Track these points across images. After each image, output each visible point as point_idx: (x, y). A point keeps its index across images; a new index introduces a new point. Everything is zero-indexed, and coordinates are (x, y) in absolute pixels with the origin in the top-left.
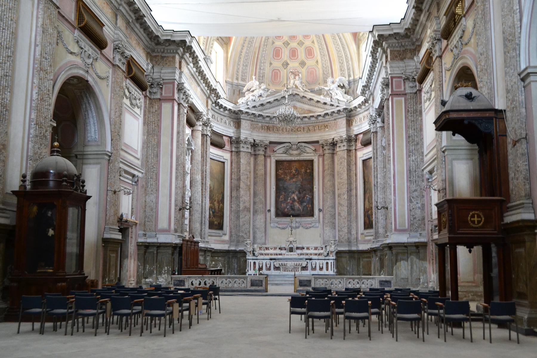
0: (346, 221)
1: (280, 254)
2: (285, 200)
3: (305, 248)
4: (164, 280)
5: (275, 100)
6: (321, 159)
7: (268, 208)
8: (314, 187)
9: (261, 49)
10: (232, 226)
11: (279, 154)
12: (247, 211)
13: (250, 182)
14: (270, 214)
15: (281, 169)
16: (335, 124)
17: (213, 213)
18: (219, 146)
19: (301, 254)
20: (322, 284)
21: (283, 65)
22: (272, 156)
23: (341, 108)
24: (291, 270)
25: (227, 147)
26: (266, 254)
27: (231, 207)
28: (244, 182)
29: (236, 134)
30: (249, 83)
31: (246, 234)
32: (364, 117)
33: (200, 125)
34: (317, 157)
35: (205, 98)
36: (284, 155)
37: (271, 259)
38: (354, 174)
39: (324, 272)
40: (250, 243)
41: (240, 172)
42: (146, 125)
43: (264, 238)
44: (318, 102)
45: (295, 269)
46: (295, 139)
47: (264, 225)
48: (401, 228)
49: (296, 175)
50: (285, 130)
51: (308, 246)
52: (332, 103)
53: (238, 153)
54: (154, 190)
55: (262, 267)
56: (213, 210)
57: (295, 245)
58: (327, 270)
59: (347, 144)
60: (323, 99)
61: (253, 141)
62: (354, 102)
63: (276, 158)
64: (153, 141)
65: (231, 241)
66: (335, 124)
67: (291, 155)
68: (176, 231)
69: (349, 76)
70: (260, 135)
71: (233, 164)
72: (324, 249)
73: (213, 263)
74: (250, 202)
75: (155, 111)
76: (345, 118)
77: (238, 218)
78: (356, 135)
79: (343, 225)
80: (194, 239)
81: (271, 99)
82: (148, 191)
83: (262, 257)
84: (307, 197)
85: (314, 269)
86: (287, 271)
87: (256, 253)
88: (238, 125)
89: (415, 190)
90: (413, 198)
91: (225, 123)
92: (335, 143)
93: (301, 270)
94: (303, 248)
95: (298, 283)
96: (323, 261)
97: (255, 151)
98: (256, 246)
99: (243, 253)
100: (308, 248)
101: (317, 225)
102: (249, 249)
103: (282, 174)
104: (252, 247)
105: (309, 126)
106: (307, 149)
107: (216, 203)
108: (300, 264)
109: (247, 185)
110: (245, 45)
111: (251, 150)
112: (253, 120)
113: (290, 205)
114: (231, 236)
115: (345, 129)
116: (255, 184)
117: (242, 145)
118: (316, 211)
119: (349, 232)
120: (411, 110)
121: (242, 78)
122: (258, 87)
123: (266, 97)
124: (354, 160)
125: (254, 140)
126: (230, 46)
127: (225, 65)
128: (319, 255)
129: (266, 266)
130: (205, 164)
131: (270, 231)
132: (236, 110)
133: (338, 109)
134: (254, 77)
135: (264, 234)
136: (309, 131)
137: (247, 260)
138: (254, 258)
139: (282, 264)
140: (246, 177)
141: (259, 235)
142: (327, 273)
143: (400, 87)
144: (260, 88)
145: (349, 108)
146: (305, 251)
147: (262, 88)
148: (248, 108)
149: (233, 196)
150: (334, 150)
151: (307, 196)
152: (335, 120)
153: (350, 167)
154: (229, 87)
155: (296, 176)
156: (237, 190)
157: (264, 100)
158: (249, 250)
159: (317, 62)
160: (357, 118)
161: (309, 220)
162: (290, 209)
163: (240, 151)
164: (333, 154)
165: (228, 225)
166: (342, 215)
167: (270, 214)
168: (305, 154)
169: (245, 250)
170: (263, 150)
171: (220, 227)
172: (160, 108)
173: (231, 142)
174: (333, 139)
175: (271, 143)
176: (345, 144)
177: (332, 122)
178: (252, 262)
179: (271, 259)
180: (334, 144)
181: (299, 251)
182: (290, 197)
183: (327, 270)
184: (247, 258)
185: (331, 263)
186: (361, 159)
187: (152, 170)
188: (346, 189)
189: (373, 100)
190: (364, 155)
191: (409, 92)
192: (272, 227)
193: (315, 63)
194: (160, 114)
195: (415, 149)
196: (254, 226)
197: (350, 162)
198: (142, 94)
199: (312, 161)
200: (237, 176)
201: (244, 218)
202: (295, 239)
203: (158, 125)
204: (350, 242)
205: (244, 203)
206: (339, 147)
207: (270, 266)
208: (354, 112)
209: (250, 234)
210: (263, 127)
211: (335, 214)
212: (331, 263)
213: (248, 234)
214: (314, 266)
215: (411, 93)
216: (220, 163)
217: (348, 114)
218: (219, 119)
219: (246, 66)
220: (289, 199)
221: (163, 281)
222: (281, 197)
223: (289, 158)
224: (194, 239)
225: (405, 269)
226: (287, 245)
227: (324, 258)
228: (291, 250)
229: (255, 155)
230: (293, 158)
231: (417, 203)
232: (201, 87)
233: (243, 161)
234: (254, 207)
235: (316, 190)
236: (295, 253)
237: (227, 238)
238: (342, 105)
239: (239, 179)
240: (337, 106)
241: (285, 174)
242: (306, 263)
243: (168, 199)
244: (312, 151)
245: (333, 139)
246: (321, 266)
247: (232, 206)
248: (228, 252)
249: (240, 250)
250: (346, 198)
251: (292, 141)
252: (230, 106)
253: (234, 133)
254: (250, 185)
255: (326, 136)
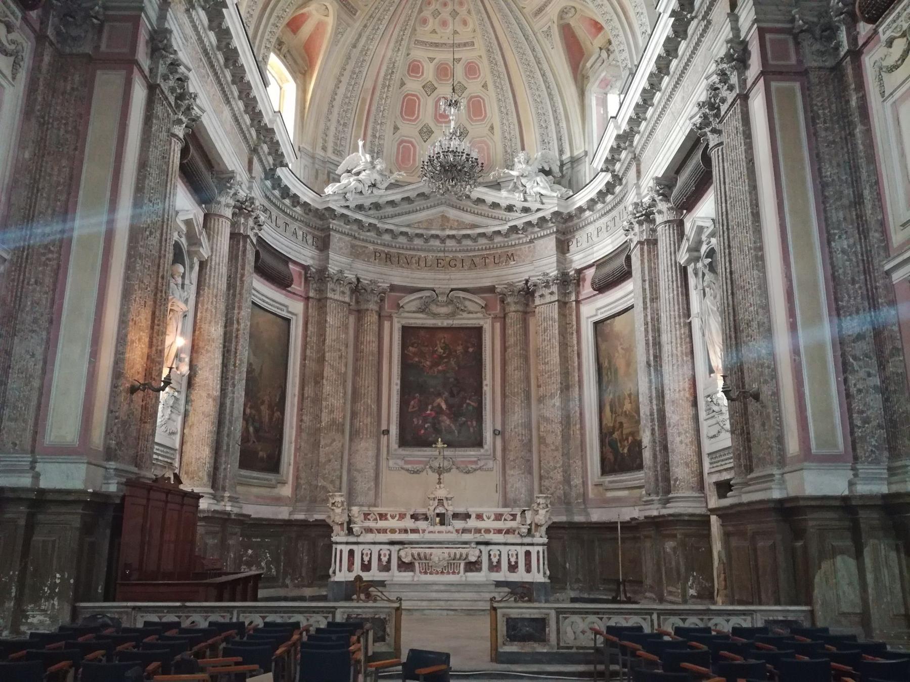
0: (558, 454)
1: (414, 531)
2: (422, 407)
3: (473, 516)
4: (47, 621)
5: (403, 199)
6: (498, 325)
7: (384, 427)
8: (484, 383)
9: (377, 93)
10: (301, 465)
11: (408, 312)
12: (337, 430)
13: (346, 366)
14: (388, 440)
15: (412, 346)
16: (530, 251)
17: (256, 431)
18: (281, 281)
19: (465, 531)
20: (583, 632)
21: (420, 132)
22: (394, 315)
23: (547, 214)
24: (439, 570)
25: (298, 287)
26: (379, 531)
27: (302, 420)
28: (332, 367)
29: (318, 262)
30: (351, 155)
31: (332, 482)
32: (599, 231)
33: (227, 205)
34: (489, 321)
35: (246, 150)
36: (421, 315)
37: (392, 543)
38: (576, 352)
39: (521, 576)
40: (342, 503)
41: (324, 344)
42: (33, 120)
43: (372, 493)
44: (495, 205)
45: (450, 566)
46: (445, 282)
47: (373, 463)
48: (825, 451)
49: (445, 357)
50: (422, 264)
51: (479, 510)
52: (526, 205)
53: (322, 302)
54: (43, 321)
55: (370, 561)
56: (257, 425)
57: (450, 508)
58: (528, 570)
59: (559, 290)
60: (506, 198)
61: (354, 280)
62: (577, 197)
63: (404, 322)
64: (55, 172)
65: (296, 500)
66: (530, 251)
67: (435, 315)
68: (110, 454)
69: (561, 152)
70: (371, 269)
71: (309, 326)
72: (518, 518)
73: (250, 552)
74: (344, 410)
75: (73, 89)
76: (554, 236)
77: (316, 445)
78: (579, 272)
79: (552, 463)
80: (181, 487)
81: (396, 195)
82: (23, 323)
83: (370, 537)
84: (469, 404)
85: (495, 567)
86: (431, 573)
87: (356, 528)
88: (323, 245)
89: (859, 334)
90: (855, 358)
91: (295, 234)
92: (532, 288)
93: (466, 571)
94: (467, 516)
95: (502, 629)
96: (518, 548)
97: (357, 302)
98: (355, 510)
99: (325, 528)
100: (479, 517)
101: (491, 464)
102: (338, 516)
103: (415, 354)
104: (346, 511)
105: (474, 256)
106: (467, 303)
107: (264, 409)
108: (464, 556)
109: (338, 374)
110: (342, 79)
111: (351, 299)
112: (356, 235)
113: (430, 420)
114: (297, 487)
115: (554, 259)
116: (356, 372)
117: (330, 285)
118: (488, 435)
119: (567, 480)
120: (824, 114)
121: (335, 149)
122: (369, 166)
123: (387, 189)
124: (574, 323)
125: (358, 279)
126: (311, 77)
127: (299, 116)
128: (508, 532)
129: (380, 559)
130: (236, 305)
131: (387, 477)
132: (320, 207)
133: (540, 214)
134: (361, 143)
135: (372, 484)
136: (473, 267)
137: (334, 546)
138: (352, 539)
139: (419, 554)
140: (337, 354)
141: (364, 485)
142: (528, 578)
143: (787, 57)
144: (374, 167)
145: (565, 211)
146: (472, 523)
147: (378, 167)
148: (347, 207)
149: (306, 395)
150: (527, 305)
151: (468, 401)
152: (531, 241)
153: (564, 337)
154: (307, 163)
155: (446, 360)
156: (317, 383)
157: (383, 195)
158: (338, 519)
159: (492, 128)
160: (581, 236)
161: (472, 453)
162: (431, 430)
163: (327, 298)
164: (525, 313)
165: (292, 462)
166: (549, 440)
167: (388, 440)
168: (465, 315)
169: (329, 521)
170: (376, 302)
171: (273, 465)
172: (88, 84)
173: (306, 279)
174: (527, 281)
175: (393, 288)
176: (554, 288)
177: (523, 247)
178: (346, 549)
179: (392, 543)
180: (528, 292)
181: (459, 524)
182: (432, 404)
183: (528, 570)
184: (334, 539)
185: (538, 552)
186: (590, 320)
187: (43, 259)
188: (559, 386)
189: (639, 172)
190: (599, 312)
191: (815, 64)
192: (390, 469)
193: (486, 131)
194: (86, 101)
195: (845, 219)
196: (350, 464)
197: (566, 329)
198: (25, 19)
199: (479, 330)
200: (318, 352)
201: (331, 444)
202: (449, 493)
203: (75, 128)
204: (568, 503)
205: (332, 412)
206: (542, 296)
207: (389, 561)
208: (576, 221)
209: (341, 483)
210: (378, 255)
211: (530, 441)
212: (538, 552)
213: (337, 483)
214: (495, 560)
215: (820, 68)
216: (279, 320)
217: (561, 226)
218: (280, 222)
219: (345, 125)
220: (430, 407)
221: (41, 622)
222: (412, 402)
223: (430, 322)
224: (181, 487)
225: (850, 584)
226: (432, 508)
227: (519, 541)
228: (442, 519)
229: (359, 311)
230: (439, 323)
231: (869, 375)
232: (232, 109)
233: (332, 320)
234: (352, 425)
235: (487, 389)
236: (450, 528)
237: (286, 491)
238: (550, 206)
239: (321, 360)
240: (538, 210)
241: (422, 355)
242: (477, 553)
243: (88, 350)
244: (479, 309)
245: (527, 281)
246: (513, 560)
247: (304, 418)
248: (288, 524)
249: (316, 520)
250: (558, 404)
251: (437, 286)
252: (307, 195)
253: (313, 258)
254: (345, 373)
255: (510, 277)
